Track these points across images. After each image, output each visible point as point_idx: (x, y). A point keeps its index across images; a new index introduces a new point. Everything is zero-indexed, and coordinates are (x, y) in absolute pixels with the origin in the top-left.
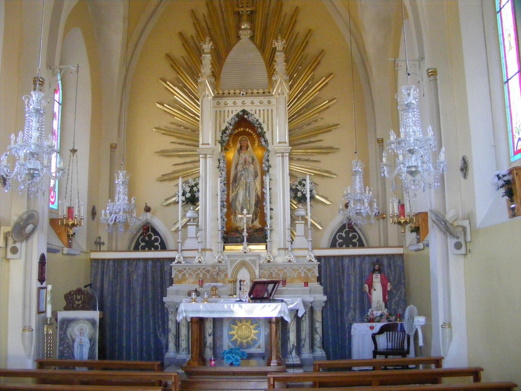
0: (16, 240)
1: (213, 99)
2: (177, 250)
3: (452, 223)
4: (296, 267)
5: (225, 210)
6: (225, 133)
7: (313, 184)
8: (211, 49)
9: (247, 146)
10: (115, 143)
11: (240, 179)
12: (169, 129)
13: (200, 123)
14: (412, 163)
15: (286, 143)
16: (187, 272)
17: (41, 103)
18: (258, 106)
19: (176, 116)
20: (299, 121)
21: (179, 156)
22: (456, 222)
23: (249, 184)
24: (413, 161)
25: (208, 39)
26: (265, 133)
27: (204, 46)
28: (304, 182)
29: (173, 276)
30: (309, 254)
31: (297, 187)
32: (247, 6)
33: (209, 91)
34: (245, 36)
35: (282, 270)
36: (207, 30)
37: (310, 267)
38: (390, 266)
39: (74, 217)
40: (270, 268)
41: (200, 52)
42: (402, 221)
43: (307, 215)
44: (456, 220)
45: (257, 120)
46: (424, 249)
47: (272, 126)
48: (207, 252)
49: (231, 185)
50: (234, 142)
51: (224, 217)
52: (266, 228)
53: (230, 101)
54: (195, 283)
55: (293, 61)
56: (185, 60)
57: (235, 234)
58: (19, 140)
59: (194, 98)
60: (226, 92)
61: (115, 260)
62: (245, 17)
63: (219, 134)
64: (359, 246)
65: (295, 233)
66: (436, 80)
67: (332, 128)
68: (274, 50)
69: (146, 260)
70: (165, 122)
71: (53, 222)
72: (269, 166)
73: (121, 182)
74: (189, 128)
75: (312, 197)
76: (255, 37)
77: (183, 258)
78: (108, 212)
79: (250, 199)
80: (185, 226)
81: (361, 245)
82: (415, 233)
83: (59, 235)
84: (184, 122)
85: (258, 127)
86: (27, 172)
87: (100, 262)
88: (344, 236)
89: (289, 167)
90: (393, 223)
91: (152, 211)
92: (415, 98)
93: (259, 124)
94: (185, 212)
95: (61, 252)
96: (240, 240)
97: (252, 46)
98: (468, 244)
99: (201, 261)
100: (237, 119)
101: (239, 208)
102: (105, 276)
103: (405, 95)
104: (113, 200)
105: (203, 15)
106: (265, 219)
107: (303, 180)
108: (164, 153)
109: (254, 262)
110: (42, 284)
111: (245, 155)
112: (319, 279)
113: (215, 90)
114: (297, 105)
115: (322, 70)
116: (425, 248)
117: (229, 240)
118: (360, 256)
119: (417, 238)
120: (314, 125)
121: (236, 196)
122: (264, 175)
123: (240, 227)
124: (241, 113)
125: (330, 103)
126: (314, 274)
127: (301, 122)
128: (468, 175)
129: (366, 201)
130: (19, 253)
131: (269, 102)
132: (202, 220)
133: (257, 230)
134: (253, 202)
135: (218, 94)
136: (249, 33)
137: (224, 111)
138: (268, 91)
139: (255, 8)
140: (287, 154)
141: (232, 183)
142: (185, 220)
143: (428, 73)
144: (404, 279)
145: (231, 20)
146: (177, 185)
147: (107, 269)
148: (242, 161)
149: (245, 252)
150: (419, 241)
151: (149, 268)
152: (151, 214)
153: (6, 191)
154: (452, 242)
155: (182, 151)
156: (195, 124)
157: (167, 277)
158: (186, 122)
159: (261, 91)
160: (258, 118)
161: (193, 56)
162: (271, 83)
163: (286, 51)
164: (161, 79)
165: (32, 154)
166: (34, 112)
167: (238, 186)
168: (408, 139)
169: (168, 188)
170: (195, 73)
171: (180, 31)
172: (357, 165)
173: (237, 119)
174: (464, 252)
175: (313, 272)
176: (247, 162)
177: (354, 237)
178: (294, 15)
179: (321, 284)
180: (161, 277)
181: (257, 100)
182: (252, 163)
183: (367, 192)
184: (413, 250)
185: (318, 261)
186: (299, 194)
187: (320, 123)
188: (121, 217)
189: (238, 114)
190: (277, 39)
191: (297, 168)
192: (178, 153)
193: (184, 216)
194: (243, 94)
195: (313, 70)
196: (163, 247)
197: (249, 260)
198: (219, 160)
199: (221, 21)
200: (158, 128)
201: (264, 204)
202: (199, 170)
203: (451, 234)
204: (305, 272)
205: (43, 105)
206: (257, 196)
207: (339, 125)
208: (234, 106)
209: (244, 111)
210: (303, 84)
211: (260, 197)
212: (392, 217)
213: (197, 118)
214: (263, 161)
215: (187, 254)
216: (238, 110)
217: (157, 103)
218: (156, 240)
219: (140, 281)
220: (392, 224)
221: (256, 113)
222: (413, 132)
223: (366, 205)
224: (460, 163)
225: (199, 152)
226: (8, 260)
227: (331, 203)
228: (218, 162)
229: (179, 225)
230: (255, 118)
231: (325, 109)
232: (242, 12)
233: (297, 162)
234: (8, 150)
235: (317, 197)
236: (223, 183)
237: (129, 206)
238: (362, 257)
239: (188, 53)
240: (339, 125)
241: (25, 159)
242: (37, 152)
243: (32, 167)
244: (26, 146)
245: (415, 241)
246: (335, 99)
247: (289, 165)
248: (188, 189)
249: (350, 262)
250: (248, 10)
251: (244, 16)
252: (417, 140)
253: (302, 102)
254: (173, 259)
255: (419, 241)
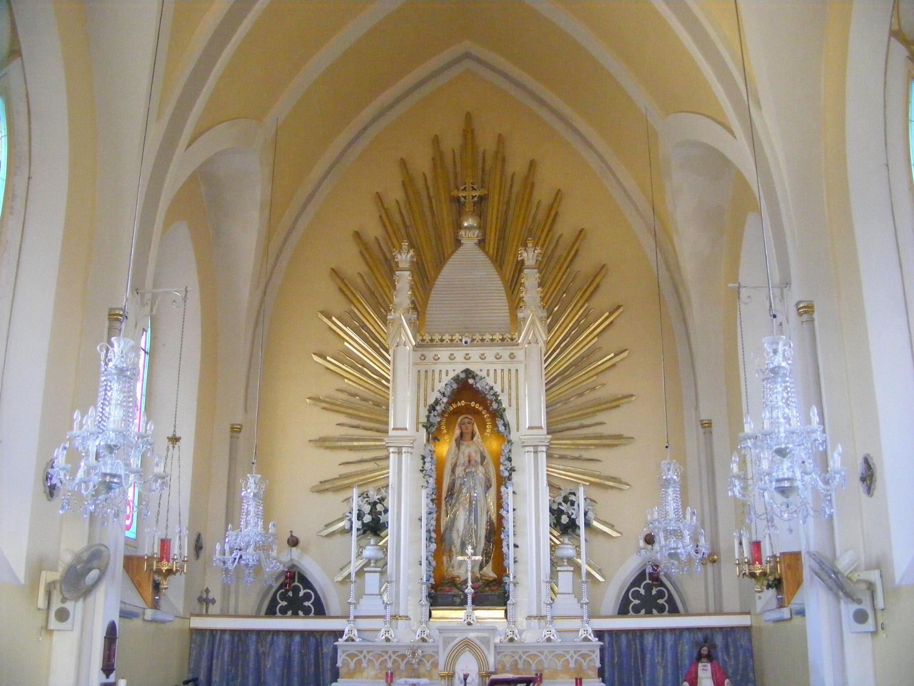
0: (67, 595)
1: (414, 350)
2: (347, 617)
3: (850, 575)
4: (560, 651)
5: (433, 546)
6: (434, 410)
7: (588, 500)
8: (412, 262)
9: (472, 433)
10: (239, 422)
11: (460, 492)
12: (333, 401)
13: (391, 392)
14: (783, 474)
15: (541, 428)
16: (365, 657)
17: (127, 357)
18: (491, 363)
19: (347, 378)
20: (564, 389)
21: (351, 448)
22: (856, 575)
23: (476, 501)
24: (785, 469)
25: (405, 244)
26: (504, 410)
27: (399, 256)
28: (572, 498)
29: (339, 664)
30: (583, 627)
31: (560, 507)
32: (473, 189)
33: (407, 335)
34: (469, 239)
35: (536, 655)
36: (403, 230)
37: (585, 651)
38: (726, 647)
39: (171, 556)
40: (513, 652)
41: (391, 268)
42: (758, 572)
43: (579, 555)
44: (855, 570)
45: (492, 388)
46: (791, 619)
47: (517, 399)
48: (400, 622)
49: (443, 502)
50: (450, 426)
51: (431, 558)
52: (506, 579)
53: (444, 354)
54: (379, 678)
55: (552, 283)
56: (365, 282)
57: (450, 591)
58: (87, 421)
59: (380, 347)
60: (437, 337)
61: (233, 632)
62: (469, 208)
63: (424, 412)
64: (669, 612)
65: (556, 588)
66: (812, 320)
67: (622, 401)
68: (520, 266)
69: (290, 633)
70: (328, 388)
71: (132, 564)
72: (512, 470)
73: (252, 494)
74: (370, 400)
75: (588, 525)
76: (487, 241)
77: (358, 630)
78: (227, 547)
79: (477, 527)
80: (360, 573)
81: (674, 611)
82: (774, 589)
83: (138, 586)
84: (361, 388)
85: (492, 401)
86: (100, 480)
87: (207, 634)
88: (643, 594)
89: (547, 471)
90: (741, 575)
91: (300, 545)
92: (785, 359)
93: (494, 395)
94: (361, 548)
95: (141, 617)
96: (458, 600)
97: (481, 256)
98: (879, 614)
99: (390, 637)
100: (455, 386)
101: (457, 543)
102: (215, 661)
103: (768, 354)
104: (237, 527)
105: (397, 202)
106: (505, 564)
107: (571, 493)
108: (325, 443)
109: (486, 641)
110: (108, 677)
111: (469, 449)
112: (601, 673)
113: (418, 335)
114: (560, 361)
115: (601, 301)
116: (795, 617)
117: (440, 600)
118: (673, 630)
119: (778, 599)
120: (590, 396)
121: (453, 521)
122: (502, 484)
123: (458, 577)
124: (463, 376)
125: (618, 358)
126: (591, 664)
127: (566, 391)
128: (874, 489)
129: (686, 533)
130: (70, 620)
131: (512, 356)
132: (393, 564)
133: (489, 583)
134: (482, 533)
135: (423, 340)
136: (476, 235)
137: (433, 371)
138: (510, 336)
139: (486, 192)
140: (544, 449)
141: (446, 498)
142: (361, 563)
143: (798, 309)
144: (754, 673)
145: (445, 211)
146: (348, 500)
147: (219, 648)
148: (463, 459)
149: (469, 624)
150: (781, 605)
151: (295, 648)
152: (299, 551)
153: (61, 512)
154: (848, 609)
155: (358, 440)
156: (381, 393)
157: (328, 665)
158: (365, 390)
159: (497, 337)
160: (492, 383)
161: (378, 276)
162: (516, 323)
163: (542, 267)
164: (322, 312)
165: (111, 449)
166: (115, 374)
167: (457, 505)
168: (776, 431)
169: (332, 504)
170: (383, 305)
171: (356, 229)
172: (669, 470)
173: (455, 386)
174: (872, 629)
175: (590, 660)
176: (473, 462)
177: (660, 595)
178: (553, 204)
179: (603, 681)
180: (317, 665)
181: (490, 353)
182: (482, 464)
183: (688, 517)
184: (769, 620)
185: (600, 640)
186: (564, 519)
187: (601, 393)
188: (250, 556)
189: (458, 376)
190: (525, 245)
191: (561, 472)
192: (350, 444)
193: (359, 555)
194: (466, 342)
195: (586, 301)
196: (320, 611)
197: (477, 638)
198: (423, 458)
199: (428, 213)
200: (316, 399)
201: (502, 536)
202: (388, 473)
203: (848, 595)
204: (576, 659)
205: (130, 360)
206: (490, 522)
207: (632, 396)
208: (451, 363)
209: (468, 372)
210: (570, 325)
211: (496, 525)
212: (738, 564)
213: (384, 382)
214: (502, 461)
215: (364, 624)
216: (457, 369)
217: (314, 354)
218: (307, 597)
219: (278, 670)
220: (739, 576)
221: (488, 375)
222: (785, 418)
223: (687, 539)
224: (859, 468)
225: (388, 443)
226: (51, 632)
227: (620, 535)
228: (422, 461)
229: (353, 568)
230: (487, 384)
231: (609, 368)
232: (465, 197)
233: (560, 461)
234: (68, 440)
235: (595, 524)
236: (430, 498)
237: (265, 537)
238: (678, 632)
239: (370, 267)
240: (632, 396)
241: (97, 456)
242: (119, 445)
243: (108, 471)
244: (99, 433)
245: (774, 604)
246: (626, 350)
247: (547, 467)
248: (367, 508)
249: (656, 642)
250: (474, 195)
251: (467, 205)
252: (793, 433)
253: (569, 357)
254: (340, 633)
255: (781, 605)
